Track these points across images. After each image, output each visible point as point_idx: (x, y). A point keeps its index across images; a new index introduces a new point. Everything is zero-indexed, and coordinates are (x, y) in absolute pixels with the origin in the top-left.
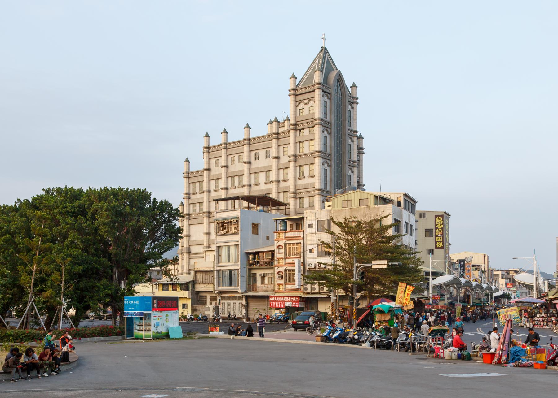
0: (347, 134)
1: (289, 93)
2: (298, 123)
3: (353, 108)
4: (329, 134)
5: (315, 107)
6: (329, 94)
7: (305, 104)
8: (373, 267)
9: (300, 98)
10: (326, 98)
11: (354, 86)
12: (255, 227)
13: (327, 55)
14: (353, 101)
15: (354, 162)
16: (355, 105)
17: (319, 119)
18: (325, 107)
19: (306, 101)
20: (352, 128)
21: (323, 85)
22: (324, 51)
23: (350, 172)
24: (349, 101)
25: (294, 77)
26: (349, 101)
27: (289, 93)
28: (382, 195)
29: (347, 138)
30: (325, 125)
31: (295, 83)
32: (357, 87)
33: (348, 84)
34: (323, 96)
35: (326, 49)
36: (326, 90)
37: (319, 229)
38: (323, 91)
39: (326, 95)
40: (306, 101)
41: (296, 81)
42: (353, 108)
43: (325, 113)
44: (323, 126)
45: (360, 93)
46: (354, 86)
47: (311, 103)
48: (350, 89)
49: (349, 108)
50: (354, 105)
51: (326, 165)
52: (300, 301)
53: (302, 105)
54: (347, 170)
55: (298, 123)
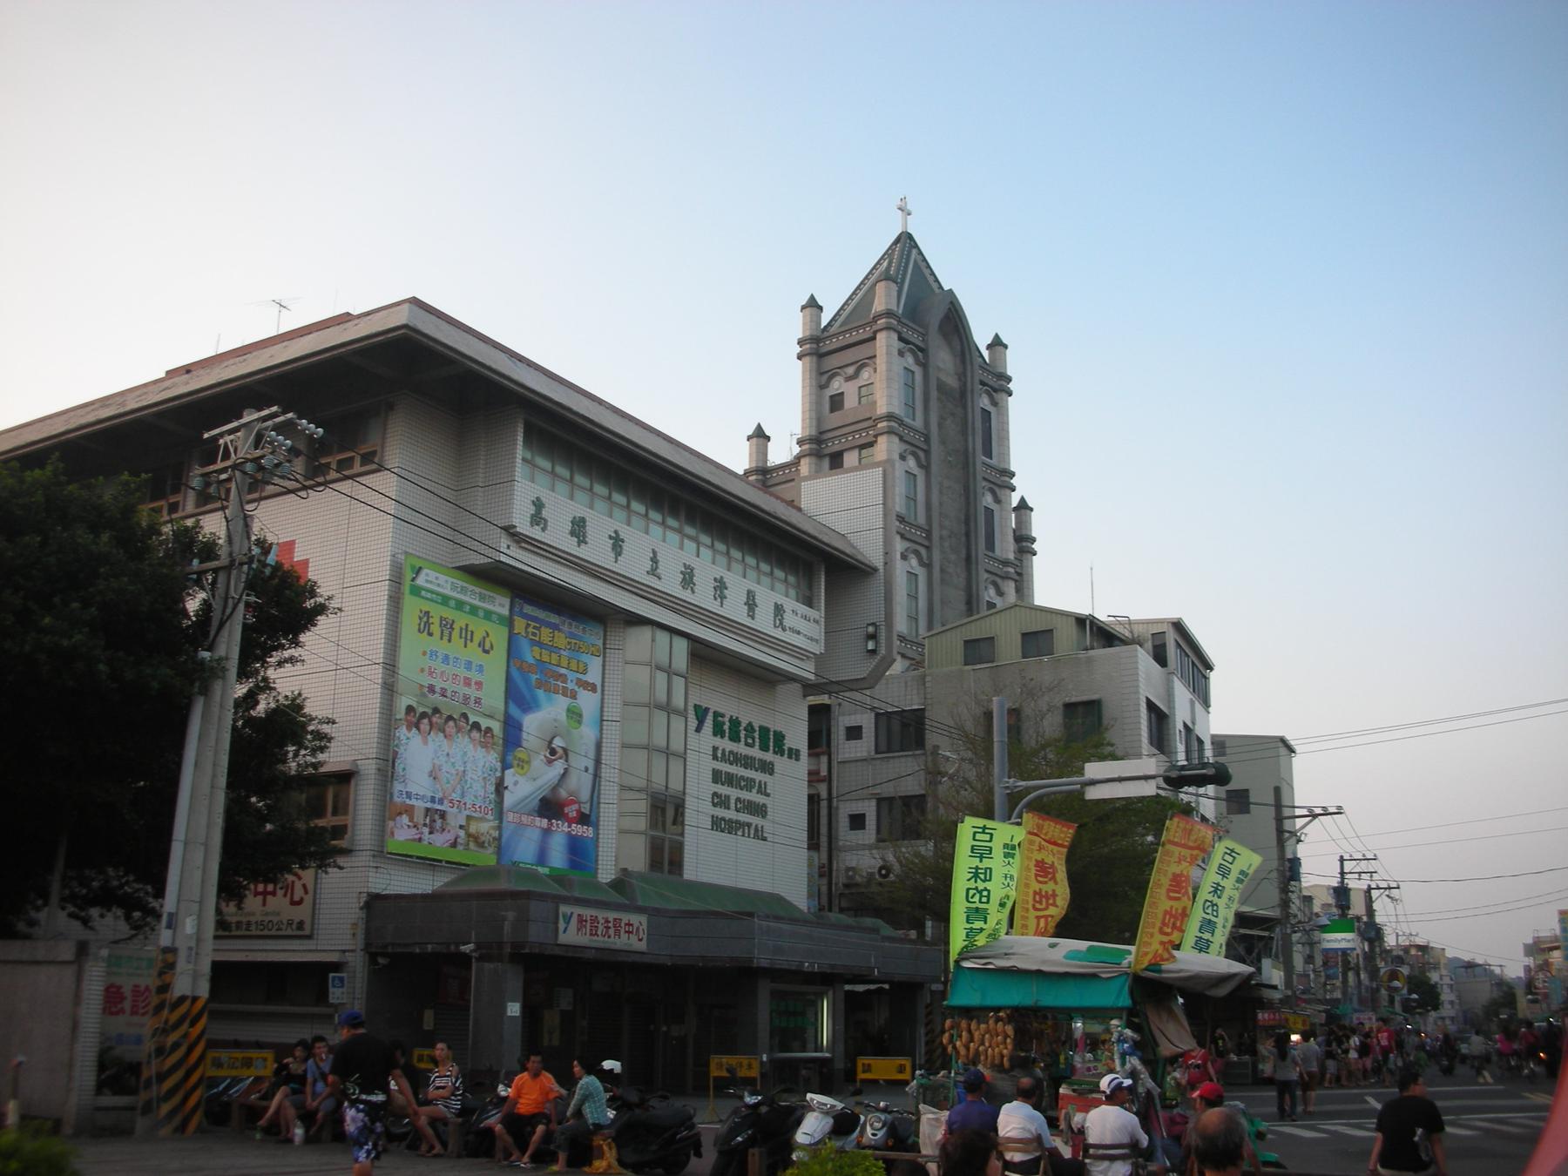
0: (979, 478)
1: (798, 349)
2: (825, 437)
3: (995, 403)
4: (920, 465)
5: (883, 384)
6: (921, 350)
7: (848, 379)
8: (1093, 794)
9: (833, 362)
10: (910, 359)
11: (997, 344)
12: (431, 673)
13: (914, 251)
14: (999, 385)
15: (1006, 563)
16: (1004, 395)
17: (890, 417)
18: (910, 386)
19: (851, 370)
20: (994, 462)
21: (899, 321)
22: (906, 241)
23: (992, 591)
24: (983, 383)
25: (813, 305)
26: (983, 383)
27: (798, 349)
28: (1102, 616)
29: (979, 490)
30: (917, 446)
31: (819, 323)
32: (1006, 347)
33: (981, 339)
34: (901, 353)
35: (910, 237)
36: (909, 335)
37: (883, 747)
38: (901, 339)
39: (911, 350)
40: (851, 370)
41: (819, 318)
42: (995, 403)
43: (910, 406)
44: (901, 439)
45: (1014, 365)
46: (997, 344)
47: (865, 374)
48: (986, 354)
49: (984, 402)
50: (999, 396)
51: (914, 562)
52: (1215, 799)
53: (837, 385)
54: (982, 586)
55: (825, 437)
